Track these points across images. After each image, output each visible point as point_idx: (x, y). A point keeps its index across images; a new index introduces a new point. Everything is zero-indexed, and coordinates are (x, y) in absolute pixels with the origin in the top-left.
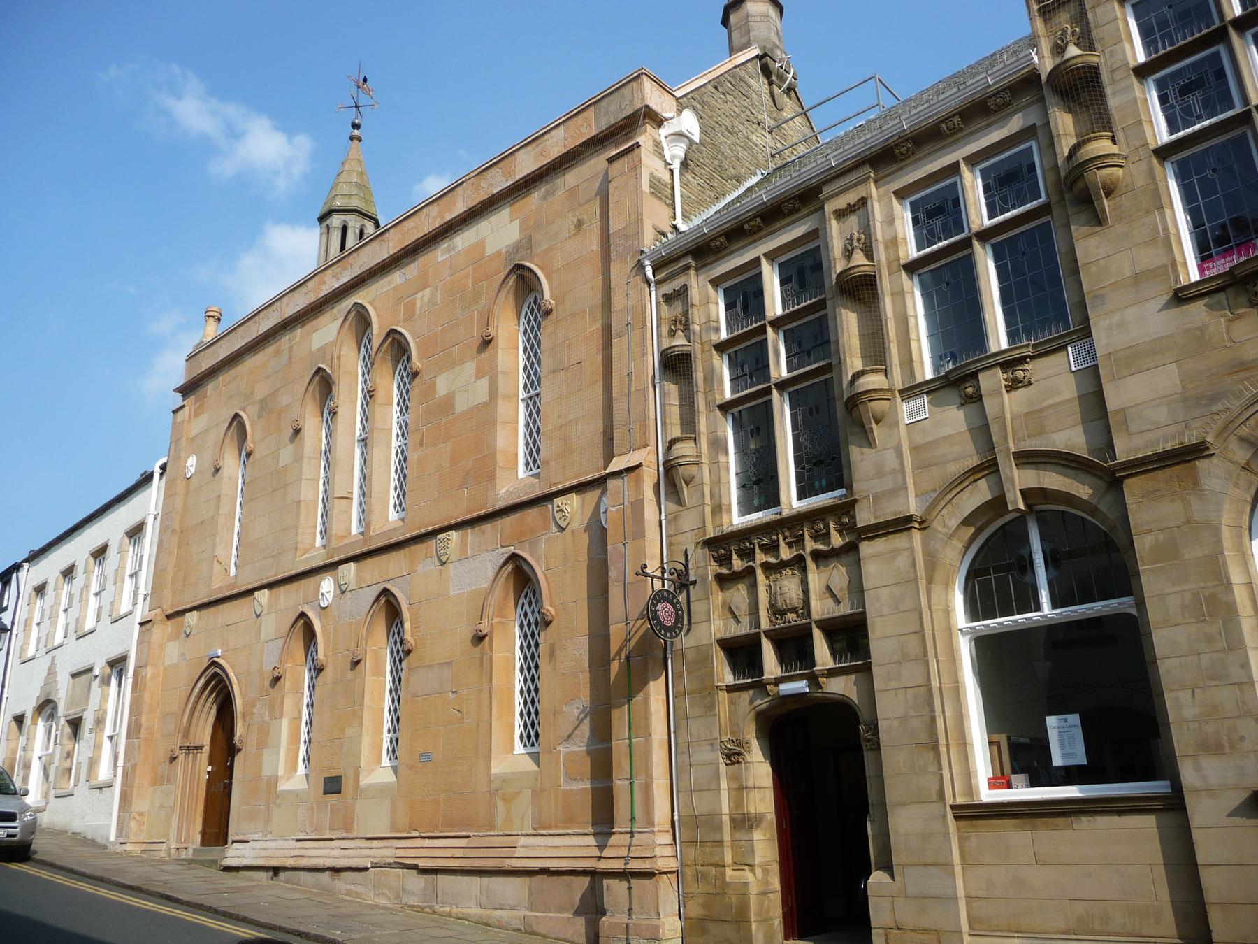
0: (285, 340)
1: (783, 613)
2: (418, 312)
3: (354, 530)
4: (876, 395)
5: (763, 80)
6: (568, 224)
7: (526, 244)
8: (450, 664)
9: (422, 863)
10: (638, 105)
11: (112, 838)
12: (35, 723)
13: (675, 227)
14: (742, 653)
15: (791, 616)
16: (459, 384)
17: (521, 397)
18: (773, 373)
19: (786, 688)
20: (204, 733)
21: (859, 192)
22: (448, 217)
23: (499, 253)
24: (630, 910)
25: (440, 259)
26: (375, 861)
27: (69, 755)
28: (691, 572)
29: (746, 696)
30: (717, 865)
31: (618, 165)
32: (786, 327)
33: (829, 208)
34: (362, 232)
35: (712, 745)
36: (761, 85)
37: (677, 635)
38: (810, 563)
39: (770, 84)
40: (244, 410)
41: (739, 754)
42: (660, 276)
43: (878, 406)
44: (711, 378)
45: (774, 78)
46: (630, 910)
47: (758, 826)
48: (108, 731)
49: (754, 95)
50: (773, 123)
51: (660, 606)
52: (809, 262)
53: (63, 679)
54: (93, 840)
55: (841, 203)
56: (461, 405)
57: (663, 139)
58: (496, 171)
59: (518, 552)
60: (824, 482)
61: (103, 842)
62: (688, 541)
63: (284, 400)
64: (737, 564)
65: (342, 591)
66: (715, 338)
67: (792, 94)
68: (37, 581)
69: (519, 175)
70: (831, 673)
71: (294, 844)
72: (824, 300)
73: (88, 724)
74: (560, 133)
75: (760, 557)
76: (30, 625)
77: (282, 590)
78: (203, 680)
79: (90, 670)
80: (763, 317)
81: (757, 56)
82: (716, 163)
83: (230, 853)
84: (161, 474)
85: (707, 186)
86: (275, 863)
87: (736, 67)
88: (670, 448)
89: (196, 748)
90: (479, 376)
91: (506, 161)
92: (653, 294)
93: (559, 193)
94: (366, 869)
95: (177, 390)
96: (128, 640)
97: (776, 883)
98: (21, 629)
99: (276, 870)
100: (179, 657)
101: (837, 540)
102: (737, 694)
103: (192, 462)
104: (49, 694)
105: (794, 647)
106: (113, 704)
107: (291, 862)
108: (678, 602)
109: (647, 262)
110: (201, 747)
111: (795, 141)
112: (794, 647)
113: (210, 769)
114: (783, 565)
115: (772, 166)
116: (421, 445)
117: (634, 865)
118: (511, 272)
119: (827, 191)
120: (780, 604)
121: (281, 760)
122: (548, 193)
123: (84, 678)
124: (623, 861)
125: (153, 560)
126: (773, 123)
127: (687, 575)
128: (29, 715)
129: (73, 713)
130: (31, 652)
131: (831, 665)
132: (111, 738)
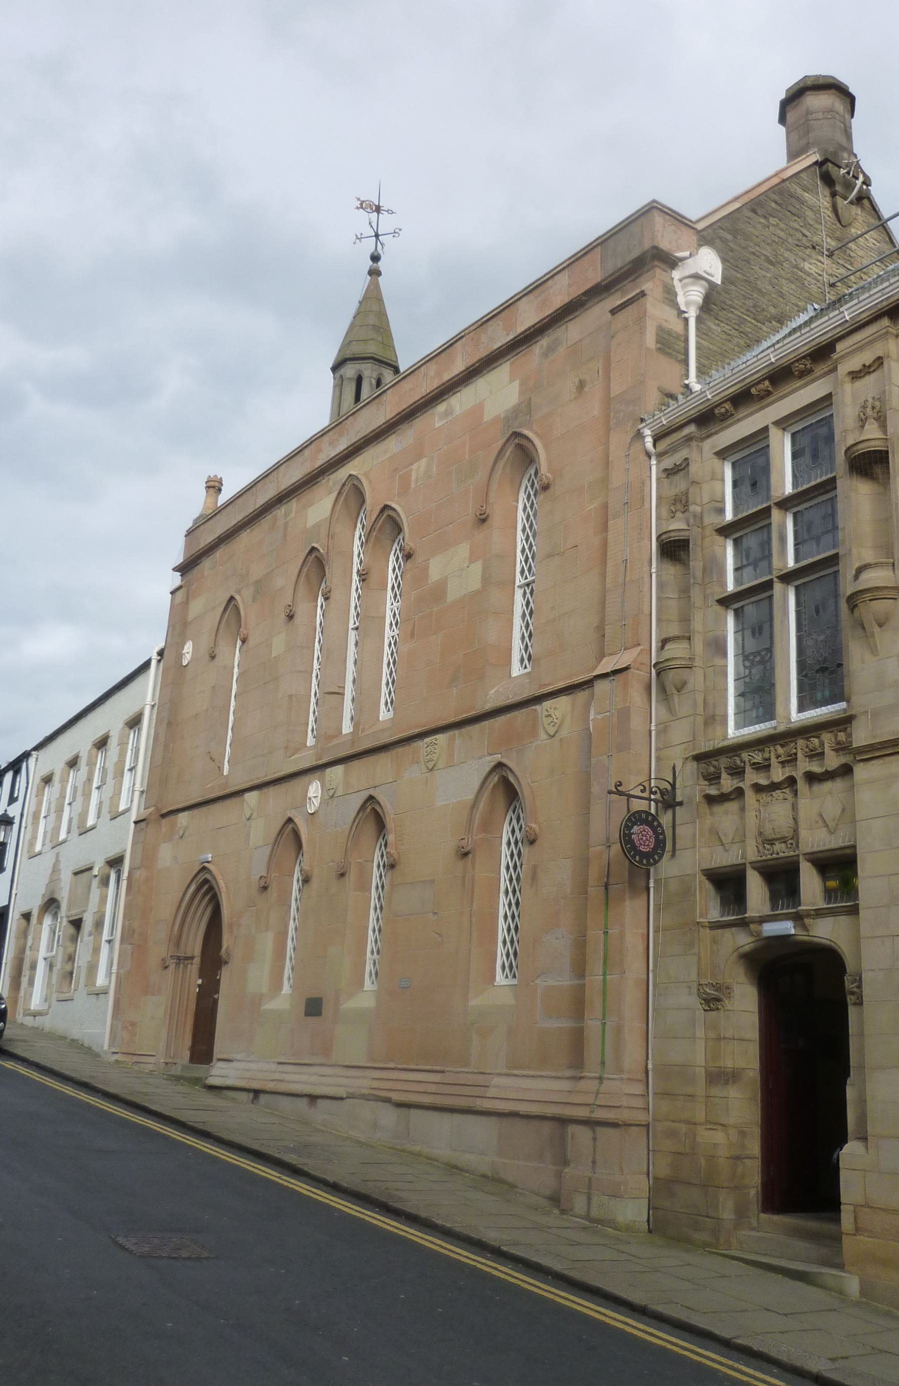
0: (280, 512)
1: (771, 842)
2: (413, 485)
3: (347, 727)
4: (879, 594)
5: (823, 192)
6: (569, 386)
7: (524, 410)
8: (432, 882)
9: (395, 1097)
10: (647, 246)
11: (106, 1047)
12: (40, 922)
13: (687, 386)
14: (728, 884)
15: (778, 847)
16: (455, 569)
17: (517, 583)
18: (776, 562)
19: (772, 929)
20: (194, 945)
21: (878, 350)
22: (447, 377)
23: (496, 420)
24: (594, 1162)
25: (437, 425)
26: (351, 1090)
27: (71, 958)
28: (679, 792)
29: (727, 933)
30: (688, 1122)
31: (622, 316)
32: (795, 510)
33: (844, 368)
34: (379, 383)
35: (690, 988)
36: (821, 199)
37: (656, 862)
38: (801, 785)
39: (834, 195)
40: (239, 592)
41: (718, 1000)
42: (663, 445)
43: (879, 606)
44: (715, 567)
45: (838, 188)
46: (594, 1162)
47: (734, 1082)
48: (105, 936)
49: (809, 213)
50: (833, 244)
51: (635, 829)
52: (823, 431)
53: (66, 876)
54: (90, 1048)
55: (855, 363)
56: (454, 593)
57: (676, 283)
58: (498, 323)
59: (504, 761)
60: (827, 693)
61: (98, 1051)
62: (677, 755)
63: (279, 582)
64: (728, 783)
65: (330, 797)
66: (719, 522)
67: (866, 202)
68: (44, 772)
69: (520, 329)
70: (819, 913)
71: (274, 1067)
72: (833, 480)
73: (88, 925)
74: (563, 280)
75: (752, 777)
76: (39, 819)
77: (271, 791)
78: (193, 887)
79: (90, 869)
80: (768, 498)
81: (816, 163)
82: (750, 303)
83: (214, 1072)
84: (159, 661)
85: (736, 333)
86: (255, 1085)
87: (784, 181)
88: (662, 648)
89: (187, 958)
90: (472, 559)
91: (506, 311)
92: (654, 468)
93: (561, 349)
94: (342, 1099)
95: (175, 569)
96: (122, 838)
97: (755, 1148)
98: (30, 822)
99: (257, 1093)
100: (174, 860)
101: (833, 761)
102: (720, 931)
103: (188, 647)
104: (53, 892)
105: (782, 879)
106: (111, 904)
107: (270, 1086)
108: (660, 825)
109: (647, 432)
110: (192, 958)
111: (866, 262)
112: (782, 879)
113: (200, 982)
114: (774, 787)
115: (830, 297)
116: (412, 636)
117: (600, 1114)
118: (507, 441)
119: (840, 347)
120: (768, 833)
121: (264, 979)
122: (551, 349)
123: (86, 874)
124: (588, 1109)
125: (149, 754)
126: (833, 244)
127: (674, 795)
128: (35, 913)
129: (74, 914)
130: (38, 848)
131: (822, 905)
132: (109, 942)
